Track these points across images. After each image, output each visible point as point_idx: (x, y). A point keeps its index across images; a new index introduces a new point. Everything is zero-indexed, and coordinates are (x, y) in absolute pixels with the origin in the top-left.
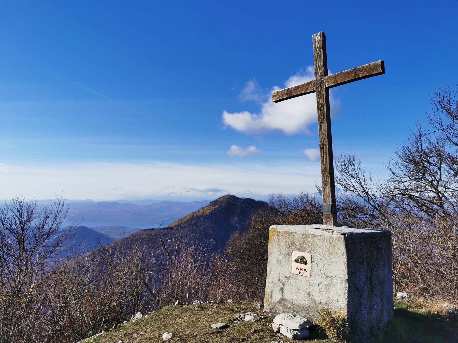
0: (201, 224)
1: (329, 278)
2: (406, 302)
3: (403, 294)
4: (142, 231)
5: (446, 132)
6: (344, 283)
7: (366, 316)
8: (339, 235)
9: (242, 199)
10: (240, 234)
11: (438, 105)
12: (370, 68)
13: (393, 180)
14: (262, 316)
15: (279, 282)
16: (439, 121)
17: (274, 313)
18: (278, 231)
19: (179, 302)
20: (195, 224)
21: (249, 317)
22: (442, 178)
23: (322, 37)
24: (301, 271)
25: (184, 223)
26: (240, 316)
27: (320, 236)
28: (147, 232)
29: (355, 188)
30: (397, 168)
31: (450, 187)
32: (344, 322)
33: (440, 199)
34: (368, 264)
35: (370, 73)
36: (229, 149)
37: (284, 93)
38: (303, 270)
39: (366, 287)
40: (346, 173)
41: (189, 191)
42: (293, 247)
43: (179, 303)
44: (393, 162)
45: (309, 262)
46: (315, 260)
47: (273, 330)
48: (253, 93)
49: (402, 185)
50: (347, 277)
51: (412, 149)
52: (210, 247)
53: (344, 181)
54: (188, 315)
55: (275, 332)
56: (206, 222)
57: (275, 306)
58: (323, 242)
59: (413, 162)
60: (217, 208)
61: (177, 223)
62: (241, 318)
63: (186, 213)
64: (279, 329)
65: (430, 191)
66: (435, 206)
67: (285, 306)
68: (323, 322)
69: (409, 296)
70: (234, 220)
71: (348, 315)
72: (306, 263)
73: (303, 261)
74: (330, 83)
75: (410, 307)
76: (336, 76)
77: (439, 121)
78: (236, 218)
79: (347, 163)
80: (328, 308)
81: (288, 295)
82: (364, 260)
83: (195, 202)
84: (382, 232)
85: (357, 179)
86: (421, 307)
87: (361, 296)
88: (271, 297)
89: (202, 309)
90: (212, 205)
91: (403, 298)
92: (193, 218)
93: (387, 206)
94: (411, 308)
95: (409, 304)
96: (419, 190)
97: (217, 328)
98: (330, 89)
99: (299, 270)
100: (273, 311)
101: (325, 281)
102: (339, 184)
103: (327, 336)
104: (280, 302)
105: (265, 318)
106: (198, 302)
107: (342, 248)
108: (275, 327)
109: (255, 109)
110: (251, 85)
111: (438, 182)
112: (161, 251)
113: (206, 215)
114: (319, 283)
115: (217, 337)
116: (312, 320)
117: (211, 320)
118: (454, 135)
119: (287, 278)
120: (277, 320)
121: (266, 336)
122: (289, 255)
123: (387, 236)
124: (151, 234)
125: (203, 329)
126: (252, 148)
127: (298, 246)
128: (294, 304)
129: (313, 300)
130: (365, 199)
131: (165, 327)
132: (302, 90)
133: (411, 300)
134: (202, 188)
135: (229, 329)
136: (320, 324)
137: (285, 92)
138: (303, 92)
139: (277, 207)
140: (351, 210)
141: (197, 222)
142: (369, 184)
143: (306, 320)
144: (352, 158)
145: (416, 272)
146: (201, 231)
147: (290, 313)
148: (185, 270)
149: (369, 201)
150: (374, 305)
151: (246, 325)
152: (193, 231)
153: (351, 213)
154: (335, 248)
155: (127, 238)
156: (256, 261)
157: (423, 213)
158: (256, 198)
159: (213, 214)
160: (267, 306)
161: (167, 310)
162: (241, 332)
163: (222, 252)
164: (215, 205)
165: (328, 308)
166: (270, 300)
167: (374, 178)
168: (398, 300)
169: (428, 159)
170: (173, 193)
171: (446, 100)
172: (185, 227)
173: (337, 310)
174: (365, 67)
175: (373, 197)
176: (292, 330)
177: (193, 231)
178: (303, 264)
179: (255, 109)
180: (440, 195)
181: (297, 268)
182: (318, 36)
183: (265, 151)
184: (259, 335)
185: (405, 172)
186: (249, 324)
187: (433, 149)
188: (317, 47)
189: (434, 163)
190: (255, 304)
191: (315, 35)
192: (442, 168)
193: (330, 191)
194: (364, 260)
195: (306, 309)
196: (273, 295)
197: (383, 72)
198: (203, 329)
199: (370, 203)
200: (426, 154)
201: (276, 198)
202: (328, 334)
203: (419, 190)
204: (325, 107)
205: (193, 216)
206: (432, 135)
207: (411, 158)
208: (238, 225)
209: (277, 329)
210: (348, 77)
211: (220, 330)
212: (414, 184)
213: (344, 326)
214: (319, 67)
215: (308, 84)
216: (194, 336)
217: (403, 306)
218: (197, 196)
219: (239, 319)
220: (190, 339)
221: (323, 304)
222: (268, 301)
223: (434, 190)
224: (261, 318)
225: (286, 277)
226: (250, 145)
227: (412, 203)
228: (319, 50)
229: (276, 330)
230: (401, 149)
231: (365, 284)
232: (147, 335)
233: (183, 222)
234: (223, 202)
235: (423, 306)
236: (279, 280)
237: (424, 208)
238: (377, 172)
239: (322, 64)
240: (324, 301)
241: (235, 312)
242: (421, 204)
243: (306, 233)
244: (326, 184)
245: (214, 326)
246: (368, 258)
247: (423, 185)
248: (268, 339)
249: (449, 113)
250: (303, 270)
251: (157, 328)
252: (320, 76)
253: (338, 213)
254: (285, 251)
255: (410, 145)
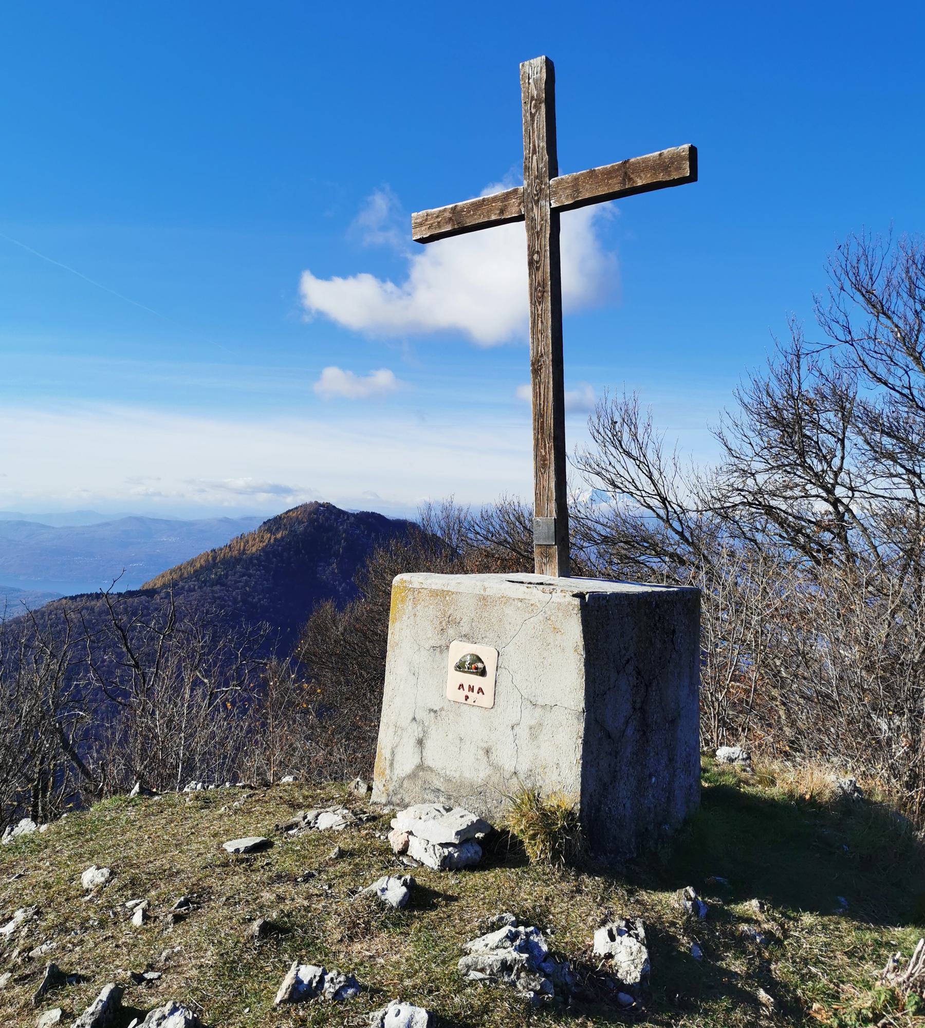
0: (236, 582)
1: (539, 710)
2: (738, 769)
3: (732, 750)
4: (64, 601)
5: (859, 348)
6: (576, 721)
7: (628, 805)
8: (569, 598)
9: (353, 515)
10: (340, 607)
11: (843, 277)
12: (662, 165)
13: (731, 467)
14: (365, 813)
15: (414, 724)
16: (842, 319)
17: (398, 805)
18: (413, 590)
19: (140, 787)
20: (219, 581)
21: (330, 819)
22: (845, 466)
23: (544, 70)
24: (470, 694)
25: (189, 578)
26: (305, 818)
27: (521, 600)
28: (80, 604)
29: (636, 487)
30: (740, 436)
31: (863, 488)
32: (572, 820)
33: (840, 516)
34: (639, 673)
35: (661, 177)
36: (317, 376)
37: (444, 218)
38: (476, 690)
39: (629, 732)
40: (616, 448)
41: (203, 491)
42: (451, 632)
43: (142, 791)
44: (730, 423)
45: (490, 670)
46: (505, 664)
47: (389, 850)
48: (384, 228)
49: (750, 482)
50: (583, 705)
51: (775, 389)
52: (256, 641)
53: (610, 468)
54: (164, 821)
55: (394, 854)
56: (250, 576)
57: (401, 786)
58: (527, 616)
59: (779, 423)
60: (283, 538)
61: (168, 578)
62: (309, 823)
63: (195, 551)
64: (406, 845)
65: (817, 496)
66: (828, 536)
67: (427, 786)
68: (519, 822)
69: (745, 756)
70: (329, 571)
71: (582, 802)
72: (483, 673)
73: (476, 668)
74: (563, 199)
75: (746, 783)
76: (576, 179)
77: (842, 319)
78: (334, 566)
79: (619, 420)
80: (534, 785)
81: (434, 757)
82: (628, 662)
83: (221, 521)
84: (676, 593)
85: (641, 462)
86: (773, 782)
87: (617, 753)
88: (392, 765)
89: (207, 803)
90: (269, 530)
91: (731, 760)
92: (215, 565)
93: (713, 535)
94: (749, 785)
95: (744, 774)
96: (789, 493)
97: (237, 850)
98: (561, 214)
99: (466, 692)
100: (395, 799)
101: (529, 718)
102: (598, 474)
103: (528, 858)
104: (413, 776)
105: (374, 819)
106: (199, 786)
107: (573, 631)
108: (396, 841)
109: (393, 270)
110: (380, 203)
111: (836, 474)
112: (120, 655)
113: (251, 558)
114: (514, 722)
115: (235, 873)
116: (493, 817)
117: (227, 832)
118: (875, 355)
119: (435, 712)
120: (402, 823)
121: (370, 866)
122: (441, 652)
123: (689, 601)
124: (92, 609)
125: (200, 854)
126: (383, 378)
127: (465, 629)
128: (449, 780)
129: (497, 768)
130: (658, 515)
131: (93, 853)
132: (490, 212)
133: (750, 766)
134: (240, 482)
135: (270, 851)
136: (510, 829)
137: (447, 215)
138: (493, 218)
139: (439, 534)
140: (625, 543)
141: (226, 576)
142: (669, 478)
143: (475, 819)
144: (631, 407)
145: (774, 699)
146: (235, 601)
147: (439, 802)
148: (179, 705)
149: (668, 521)
150: (650, 776)
151: (318, 840)
152: (215, 599)
153: (623, 552)
154: (556, 630)
155: (17, 621)
156: (362, 669)
157: (799, 553)
158: (391, 513)
159: (269, 553)
160: (381, 787)
161: (106, 809)
162: (302, 858)
163: (281, 655)
164: (277, 530)
165: (534, 785)
166: (388, 772)
167: (683, 463)
168: (717, 765)
169: (815, 416)
170: (159, 494)
171: (862, 268)
172: (191, 590)
173: (556, 789)
174: (648, 160)
175: (678, 509)
176: (438, 847)
177: (215, 599)
178: (476, 674)
179: (393, 270)
180: (841, 509)
181: (461, 686)
182: (534, 68)
183: (394, 380)
184: (350, 864)
185: (758, 449)
186: (331, 835)
187: (827, 391)
188: (532, 98)
189: (828, 427)
190: (353, 784)
191: (527, 63)
192: (846, 441)
193: (553, 485)
194: (628, 662)
195: (480, 792)
196: (397, 758)
197: (693, 178)
198: (200, 854)
199: (671, 525)
200: (811, 404)
201: (437, 513)
202: (529, 852)
203: (789, 493)
204: (548, 261)
205: (214, 558)
206: (826, 354)
207: (774, 413)
208: (340, 584)
209: (401, 846)
210: (608, 185)
211: (245, 856)
212: (779, 477)
213: (570, 830)
214: (534, 152)
215: (506, 197)
216: (171, 875)
217: (730, 780)
218: (226, 504)
219: (303, 824)
220: (159, 882)
221: (522, 776)
222: (383, 774)
223: (824, 495)
224: (360, 819)
225: (431, 710)
226: (377, 368)
227: (773, 527)
228: (535, 106)
229: (397, 848)
230: (749, 385)
231: (627, 722)
232: (40, 876)
233: (186, 575)
234: (300, 522)
235: (778, 782)
236: (414, 719)
237: (802, 539)
238: (689, 447)
239: (543, 144)
240: (523, 768)
241: (295, 806)
242: (794, 530)
243: (487, 593)
244: (544, 466)
245: (230, 847)
246: (642, 656)
247: (798, 480)
248: (373, 872)
249: (869, 301)
250: (476, 690)
251: (70, 857)
252: (536, 177)
253: (565, 542)
254: (432, 643)
255: (773, 378)
